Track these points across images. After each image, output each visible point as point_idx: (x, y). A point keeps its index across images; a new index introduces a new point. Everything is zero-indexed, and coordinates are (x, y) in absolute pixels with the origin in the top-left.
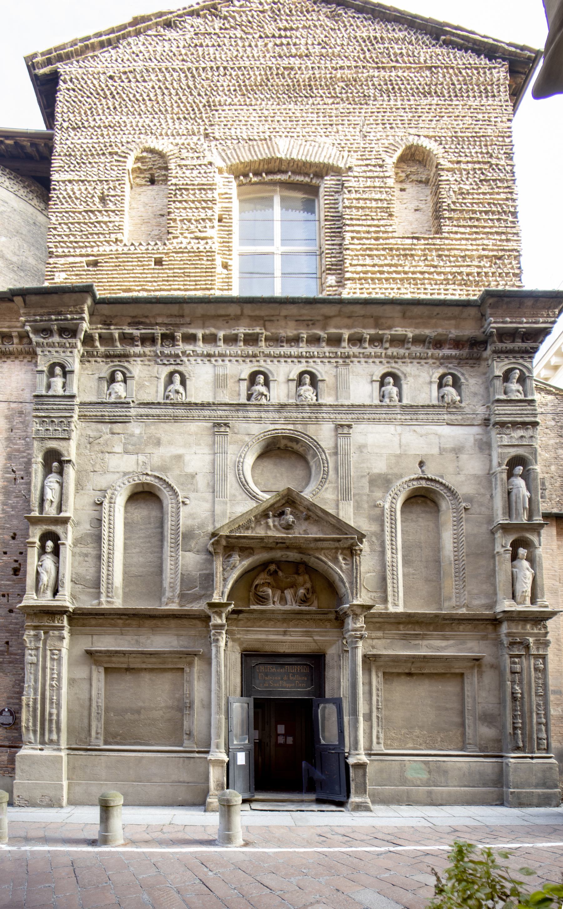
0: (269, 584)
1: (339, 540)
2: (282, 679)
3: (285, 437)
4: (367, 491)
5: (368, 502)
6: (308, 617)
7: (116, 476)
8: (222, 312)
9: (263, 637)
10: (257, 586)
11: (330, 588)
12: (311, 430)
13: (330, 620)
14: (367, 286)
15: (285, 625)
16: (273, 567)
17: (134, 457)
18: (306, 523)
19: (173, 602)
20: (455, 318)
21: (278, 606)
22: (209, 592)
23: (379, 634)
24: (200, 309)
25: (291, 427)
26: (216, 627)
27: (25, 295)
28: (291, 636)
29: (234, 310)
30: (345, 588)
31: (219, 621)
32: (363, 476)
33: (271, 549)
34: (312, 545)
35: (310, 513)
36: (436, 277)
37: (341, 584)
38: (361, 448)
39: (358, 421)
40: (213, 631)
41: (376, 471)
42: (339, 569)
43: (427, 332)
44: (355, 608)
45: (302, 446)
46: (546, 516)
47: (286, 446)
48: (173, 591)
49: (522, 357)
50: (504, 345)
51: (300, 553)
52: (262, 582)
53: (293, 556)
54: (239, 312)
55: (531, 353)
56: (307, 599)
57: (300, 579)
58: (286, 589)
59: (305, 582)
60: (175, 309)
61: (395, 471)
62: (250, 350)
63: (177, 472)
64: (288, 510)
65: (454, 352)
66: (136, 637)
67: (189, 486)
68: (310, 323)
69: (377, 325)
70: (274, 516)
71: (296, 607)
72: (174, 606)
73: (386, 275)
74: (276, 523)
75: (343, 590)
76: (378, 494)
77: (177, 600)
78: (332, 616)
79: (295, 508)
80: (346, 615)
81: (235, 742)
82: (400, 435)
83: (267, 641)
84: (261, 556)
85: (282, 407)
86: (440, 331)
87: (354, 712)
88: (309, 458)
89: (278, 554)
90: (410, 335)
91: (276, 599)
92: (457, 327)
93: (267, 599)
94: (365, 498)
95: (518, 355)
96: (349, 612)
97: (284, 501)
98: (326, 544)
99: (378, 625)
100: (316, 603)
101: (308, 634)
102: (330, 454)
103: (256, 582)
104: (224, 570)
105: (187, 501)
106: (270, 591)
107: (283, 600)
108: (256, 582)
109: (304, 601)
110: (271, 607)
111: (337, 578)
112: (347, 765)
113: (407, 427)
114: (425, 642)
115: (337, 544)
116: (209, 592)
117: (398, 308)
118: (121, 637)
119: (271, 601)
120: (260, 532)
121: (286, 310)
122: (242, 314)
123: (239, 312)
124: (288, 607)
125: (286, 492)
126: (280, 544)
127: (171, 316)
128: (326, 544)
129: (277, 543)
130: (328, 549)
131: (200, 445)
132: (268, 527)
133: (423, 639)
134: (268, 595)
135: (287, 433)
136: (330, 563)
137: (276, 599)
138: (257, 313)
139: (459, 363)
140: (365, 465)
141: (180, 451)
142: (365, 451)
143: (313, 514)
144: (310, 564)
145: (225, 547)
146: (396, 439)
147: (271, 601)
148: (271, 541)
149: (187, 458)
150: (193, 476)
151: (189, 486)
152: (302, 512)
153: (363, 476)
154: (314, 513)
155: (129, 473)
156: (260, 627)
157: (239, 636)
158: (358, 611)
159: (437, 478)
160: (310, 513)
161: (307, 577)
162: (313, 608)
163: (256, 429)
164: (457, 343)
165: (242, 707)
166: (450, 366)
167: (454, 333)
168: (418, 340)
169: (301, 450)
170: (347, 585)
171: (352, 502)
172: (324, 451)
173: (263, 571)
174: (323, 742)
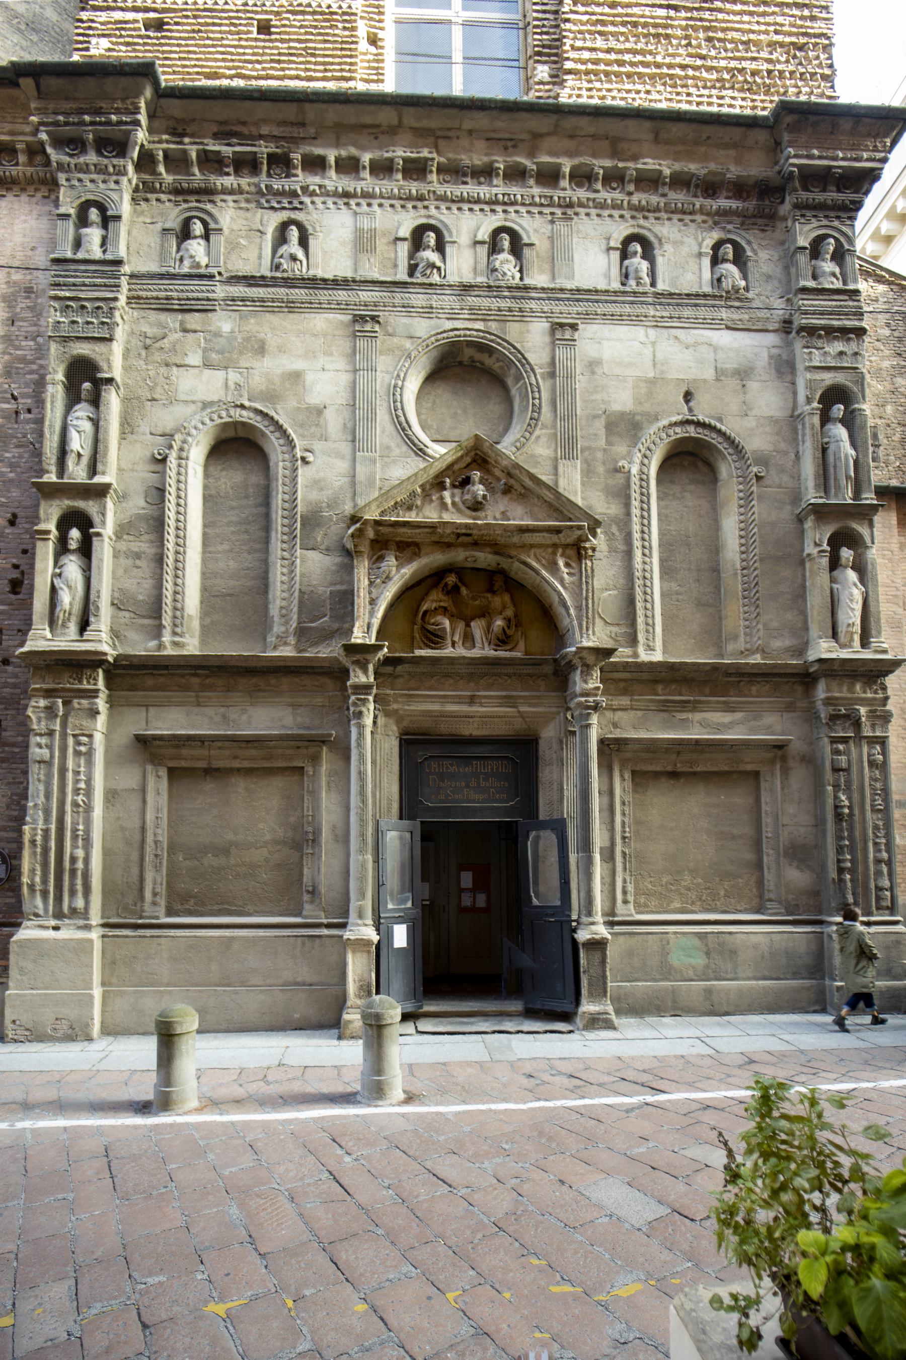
0: (445, 611)
1: (558, 531)
2: (468, 786)
3: (470, 344)
4: (602, 442)
5: (604, 463)
6: (510, 670)
7: (191, 408)
8: (367, 120)
9: (436, 707)
10: (425, 612)
12: (513, 332)
13: (544, 676)
14: (598, 85)
15: (472, 685)
16: (451, 579)
17: (221, 374)
19: (286, 644)
20: (735, 145)
21: (461, 651)
22: (346, 626)
23: (625, 701)
24: (332, 114)
25: (479, 325)
27: (39, 75)
28: (481, 705)
29: (387, 116)
30: (569, 618)
31: (363, 679)
32: (596, 417)
34: (515, 539)
36: (705, 75)
38: (593, 365)
39: (588, 317)
40: (353, 698)
41: (616, 407)
42: (559, 582)
43: (692, 167)
45: (498, 360)
46: (883, 492)
47: (472, 359)
48: (287, 623)
49: (838, 217)
50: (811, 196)
51: (497, 553)
52: (434, 605)
53: (485, 558)
54: (395, 122)
55: (851, 210)
56: (508, 637)
58: (472, 619)
59: (504, 607)
60: (290, 111)
61: (647, 407)
62: (414, 187)
63: (292, 403)
64: (476, 475)
65: (734, 204)
66: (222, 710)
67: (313, 429)
68: (509, 144)
69: (615, 153)
70: (454, 486)
72: (287, 652)
73: (628, 69)
74: (457, 499)
75: (566, 621)
76: (621, 448)
77: (292, 640)
78: (548, 669)
80: (571, 667)
81: (390, 906)
82: (654, 343)
83: (443, 715)
85: (466, 288)
86: (712, 166)
87: (586, 846)
88: (510, 381)
89: (459, 556)
90: (667, 172)
91: (456, 638)
92: (738, 161)
93: (443, 638)
94: (599, 455)
95: (832, 214)
96: (576, 661)
98: (537, 538)
99: (622, 685)
100: (522, 644)
101: (508, 701)
103: (425, 607)
104: (371, 583)
106: (447, 623)
107: (468, 639)
108: (425, 608)
109: (503, 641)
110: (448, 652)
111: (556, 599)
112: (575, 943)
113: (665, 331)
114: (698, 716)
115: (555, 539)
116: (346, 626)
117: (647, 124)
118: (196, 710)
119: (449, 641)
121: (471, 121)
122: (400, 125)
123: (395, 122)
124: (476, 653)
127: (284, 123)
128: (537, 538)
129: (458, 535)
130: (540, 546)
131: (331, 354)
132: (443, 506)
133: (694, 710)
135: (474, 337)
138: (424, 123)
139: (742, 224)
140: (598, 397)
141: (298, 365)
142: (599, 371)
143: (516, 484)
144: (512, 575)
146: (648, 351)
147: (449, 641)
148: (448, 531)
149: (309, 378)
150: (319, 411)
151: (313, 429)
152: (499, 480)
153: (596, 417)
155: (212, 403)
156: (430, 689)
157: (395, 706)
158: (590, 659)
159: (713, 422)
160: (512, 481)
161: (507, 598)
162: (517, 654)
163: (423, 327)
164: (739, 189)
165: (401, 838)
166: (730, 227)
167: (734, 171)
168: (680, 181)
169: (496, 366)
172: (533, 370)
173: (435, 585)
174: (535, 902)
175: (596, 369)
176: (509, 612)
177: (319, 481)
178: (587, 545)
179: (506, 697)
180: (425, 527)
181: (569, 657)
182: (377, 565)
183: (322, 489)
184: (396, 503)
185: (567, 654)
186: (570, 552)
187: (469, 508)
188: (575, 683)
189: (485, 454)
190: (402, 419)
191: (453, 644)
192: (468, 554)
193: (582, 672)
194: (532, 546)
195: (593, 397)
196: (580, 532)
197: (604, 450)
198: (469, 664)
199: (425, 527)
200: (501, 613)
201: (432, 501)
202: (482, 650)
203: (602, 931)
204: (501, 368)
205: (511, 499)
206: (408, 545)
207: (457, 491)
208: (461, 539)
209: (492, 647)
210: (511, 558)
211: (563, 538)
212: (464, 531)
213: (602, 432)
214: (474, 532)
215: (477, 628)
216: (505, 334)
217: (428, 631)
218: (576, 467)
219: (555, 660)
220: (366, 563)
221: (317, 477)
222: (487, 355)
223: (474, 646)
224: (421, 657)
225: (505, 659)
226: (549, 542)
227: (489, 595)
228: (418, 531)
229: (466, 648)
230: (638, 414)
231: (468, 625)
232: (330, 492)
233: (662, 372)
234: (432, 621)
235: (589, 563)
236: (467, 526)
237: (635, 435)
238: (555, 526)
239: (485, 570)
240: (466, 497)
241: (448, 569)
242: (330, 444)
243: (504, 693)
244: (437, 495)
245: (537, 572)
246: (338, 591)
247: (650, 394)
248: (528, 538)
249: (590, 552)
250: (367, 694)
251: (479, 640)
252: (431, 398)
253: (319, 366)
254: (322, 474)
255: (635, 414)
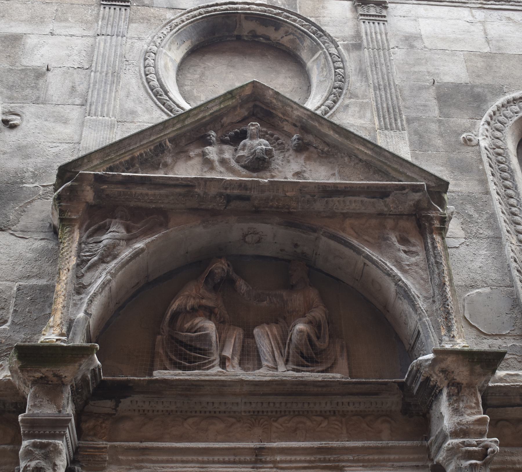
0: (209, 313)
1: (382, 193)
3: (251, 17)
4: (436, 113)
5: (441, 135)
10: (175, 315)
11: (379, 322)
15: (258, 431)
16: (220, 267)
18: (301, 159)
21: (235, 372)
26: (36, 427)
30: (419, 314)
31: (48, 411)
33: (214, 213)
34: (319, 206)
35: (309, 138)
37: (404, 306)
38: (410, 41)
40: (25, 443)
41: (448, 79)
42: (398, 268)
44: (449, 362)
45: (287, 33)
47: (254, 35)
51: (290, 225)
52: (191, 302)
53: (273, 236)
57: (297, 300)
59: (309, 308)
61: (488, 80)
64: (254, 126)
67: (28, 91)
71: (285, 372)
75: (413, 321)
76: (460, 120)
78: (392, 402)
79: (274, 127)
80: (431, 393)
82: (483, 23)
84: (190, 233)
88: (304, 55)
89: (234, 230)
91: (228, 352)
93: (206, 352)
94: (434, 127)
96: (436, 378)
97: (244, 112)
98: (353, 204)
100: (343, 363)
102: (346, 47)
103: (174, 306)
105: (15, 120)
106: (210, 327)
107: (249, 355)
108: (174, 306)
110: (214, 372)
111: (393, 288)
113: (496, 13)
115: (380, 205)
119: (216, 358)
120: (187, 170)
124: (262, 374)
125: (248, 91)
126: (234, 201)
128: (353, 204)
129: (229, 199)
130: (359, 215)
131: (66, 20)
132: (208, 163)
134: (207, 336)
136: (367, 250)
137: (228, 352)
142: (417, 44)
145: (91, 209)
146: (477, 29)
147: (216, 358)
149: (31, 41)
150: (40, 74)
152: (290, 136)
154: (321, 136)
156: (180, 439)
158: (462, 373)
160: (309, 138)
161: (313, 294)
162: (336, 376)
169: (285, 40)
170: (421, 304)
171: (406, 134)
172: (333, 41)
175: (415, 43)
176: (318, 313)
177: (25, 147)
178: (432, 214)
179: (320, 450)
180: (175, 186)
181: (425, 371)
182: (96, 238)
183: (28, 156)
184: (133, 159)
185: (420, 365)
186: (404, 224)
187: (245, 167)
188: (441, 417)
189: (267, 104)
190: (155, 83)
191: (223, 363)
192: (245, 226)
193: (449, 396)
194: (345, 216)
195: (416, 69)
196: (417, 196)
197: (440, 121)
198: (252, 394)
199: (175, 186)
200: (304, 316)
201: (190, 158)
202: (274, 370)
203: (453, 317)
204: (293, 41)
205: (308, 159)
206: (149, 212)
207: (225, 147)
208: (233, 205)
209: (291, 366)
210: (315, 231)
211: (389, 204)
212: (236, 192)
213: (434, 104)
214: (254, 194)
215: (264, 339)
216: (296, 9)
217: (181, 343)
218: (403, 139)
219: (402, 385)
220: (76, 235)
221: (25, 143)
222: (273, 28)
223: (260, 366)
224: (164, 381)
225: (315, 383)
226: (371, 210)
227: (284, 293)
228: (163, 192)
229: (244, 369)
230: (477, 86)
231: (249, 335)
232: (39, 160)
233: (500, 49)
234: (187, 326)
235: (438, 238)
236: (241, 185)
237: (479, 107)
238: (377, 186)
239: (276, 259)
240: (241, 153)
241: (218, 251)
242: (49, 108)
243: (316, 444)
244: (198, 151)
245: (359, 252)
246: (32, 287)
247: (489, 68)
248: (337, 203)
249: (437, 224)
250: (54, 436)
251: (268, 357)
252: (199, 70)
253: (48, 31)
254: (30, 139)
255: (473, 87)
